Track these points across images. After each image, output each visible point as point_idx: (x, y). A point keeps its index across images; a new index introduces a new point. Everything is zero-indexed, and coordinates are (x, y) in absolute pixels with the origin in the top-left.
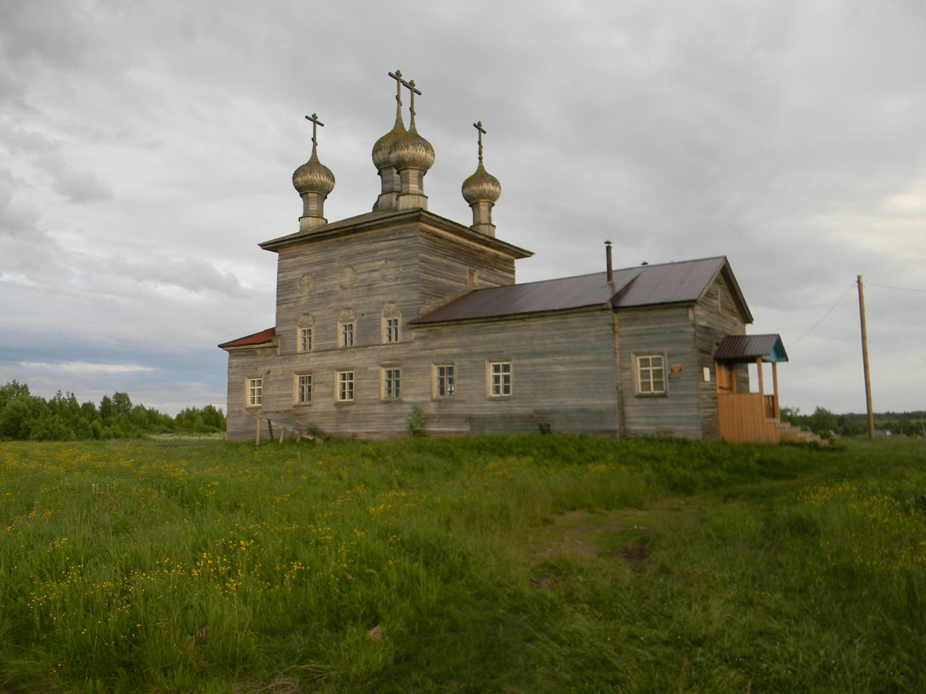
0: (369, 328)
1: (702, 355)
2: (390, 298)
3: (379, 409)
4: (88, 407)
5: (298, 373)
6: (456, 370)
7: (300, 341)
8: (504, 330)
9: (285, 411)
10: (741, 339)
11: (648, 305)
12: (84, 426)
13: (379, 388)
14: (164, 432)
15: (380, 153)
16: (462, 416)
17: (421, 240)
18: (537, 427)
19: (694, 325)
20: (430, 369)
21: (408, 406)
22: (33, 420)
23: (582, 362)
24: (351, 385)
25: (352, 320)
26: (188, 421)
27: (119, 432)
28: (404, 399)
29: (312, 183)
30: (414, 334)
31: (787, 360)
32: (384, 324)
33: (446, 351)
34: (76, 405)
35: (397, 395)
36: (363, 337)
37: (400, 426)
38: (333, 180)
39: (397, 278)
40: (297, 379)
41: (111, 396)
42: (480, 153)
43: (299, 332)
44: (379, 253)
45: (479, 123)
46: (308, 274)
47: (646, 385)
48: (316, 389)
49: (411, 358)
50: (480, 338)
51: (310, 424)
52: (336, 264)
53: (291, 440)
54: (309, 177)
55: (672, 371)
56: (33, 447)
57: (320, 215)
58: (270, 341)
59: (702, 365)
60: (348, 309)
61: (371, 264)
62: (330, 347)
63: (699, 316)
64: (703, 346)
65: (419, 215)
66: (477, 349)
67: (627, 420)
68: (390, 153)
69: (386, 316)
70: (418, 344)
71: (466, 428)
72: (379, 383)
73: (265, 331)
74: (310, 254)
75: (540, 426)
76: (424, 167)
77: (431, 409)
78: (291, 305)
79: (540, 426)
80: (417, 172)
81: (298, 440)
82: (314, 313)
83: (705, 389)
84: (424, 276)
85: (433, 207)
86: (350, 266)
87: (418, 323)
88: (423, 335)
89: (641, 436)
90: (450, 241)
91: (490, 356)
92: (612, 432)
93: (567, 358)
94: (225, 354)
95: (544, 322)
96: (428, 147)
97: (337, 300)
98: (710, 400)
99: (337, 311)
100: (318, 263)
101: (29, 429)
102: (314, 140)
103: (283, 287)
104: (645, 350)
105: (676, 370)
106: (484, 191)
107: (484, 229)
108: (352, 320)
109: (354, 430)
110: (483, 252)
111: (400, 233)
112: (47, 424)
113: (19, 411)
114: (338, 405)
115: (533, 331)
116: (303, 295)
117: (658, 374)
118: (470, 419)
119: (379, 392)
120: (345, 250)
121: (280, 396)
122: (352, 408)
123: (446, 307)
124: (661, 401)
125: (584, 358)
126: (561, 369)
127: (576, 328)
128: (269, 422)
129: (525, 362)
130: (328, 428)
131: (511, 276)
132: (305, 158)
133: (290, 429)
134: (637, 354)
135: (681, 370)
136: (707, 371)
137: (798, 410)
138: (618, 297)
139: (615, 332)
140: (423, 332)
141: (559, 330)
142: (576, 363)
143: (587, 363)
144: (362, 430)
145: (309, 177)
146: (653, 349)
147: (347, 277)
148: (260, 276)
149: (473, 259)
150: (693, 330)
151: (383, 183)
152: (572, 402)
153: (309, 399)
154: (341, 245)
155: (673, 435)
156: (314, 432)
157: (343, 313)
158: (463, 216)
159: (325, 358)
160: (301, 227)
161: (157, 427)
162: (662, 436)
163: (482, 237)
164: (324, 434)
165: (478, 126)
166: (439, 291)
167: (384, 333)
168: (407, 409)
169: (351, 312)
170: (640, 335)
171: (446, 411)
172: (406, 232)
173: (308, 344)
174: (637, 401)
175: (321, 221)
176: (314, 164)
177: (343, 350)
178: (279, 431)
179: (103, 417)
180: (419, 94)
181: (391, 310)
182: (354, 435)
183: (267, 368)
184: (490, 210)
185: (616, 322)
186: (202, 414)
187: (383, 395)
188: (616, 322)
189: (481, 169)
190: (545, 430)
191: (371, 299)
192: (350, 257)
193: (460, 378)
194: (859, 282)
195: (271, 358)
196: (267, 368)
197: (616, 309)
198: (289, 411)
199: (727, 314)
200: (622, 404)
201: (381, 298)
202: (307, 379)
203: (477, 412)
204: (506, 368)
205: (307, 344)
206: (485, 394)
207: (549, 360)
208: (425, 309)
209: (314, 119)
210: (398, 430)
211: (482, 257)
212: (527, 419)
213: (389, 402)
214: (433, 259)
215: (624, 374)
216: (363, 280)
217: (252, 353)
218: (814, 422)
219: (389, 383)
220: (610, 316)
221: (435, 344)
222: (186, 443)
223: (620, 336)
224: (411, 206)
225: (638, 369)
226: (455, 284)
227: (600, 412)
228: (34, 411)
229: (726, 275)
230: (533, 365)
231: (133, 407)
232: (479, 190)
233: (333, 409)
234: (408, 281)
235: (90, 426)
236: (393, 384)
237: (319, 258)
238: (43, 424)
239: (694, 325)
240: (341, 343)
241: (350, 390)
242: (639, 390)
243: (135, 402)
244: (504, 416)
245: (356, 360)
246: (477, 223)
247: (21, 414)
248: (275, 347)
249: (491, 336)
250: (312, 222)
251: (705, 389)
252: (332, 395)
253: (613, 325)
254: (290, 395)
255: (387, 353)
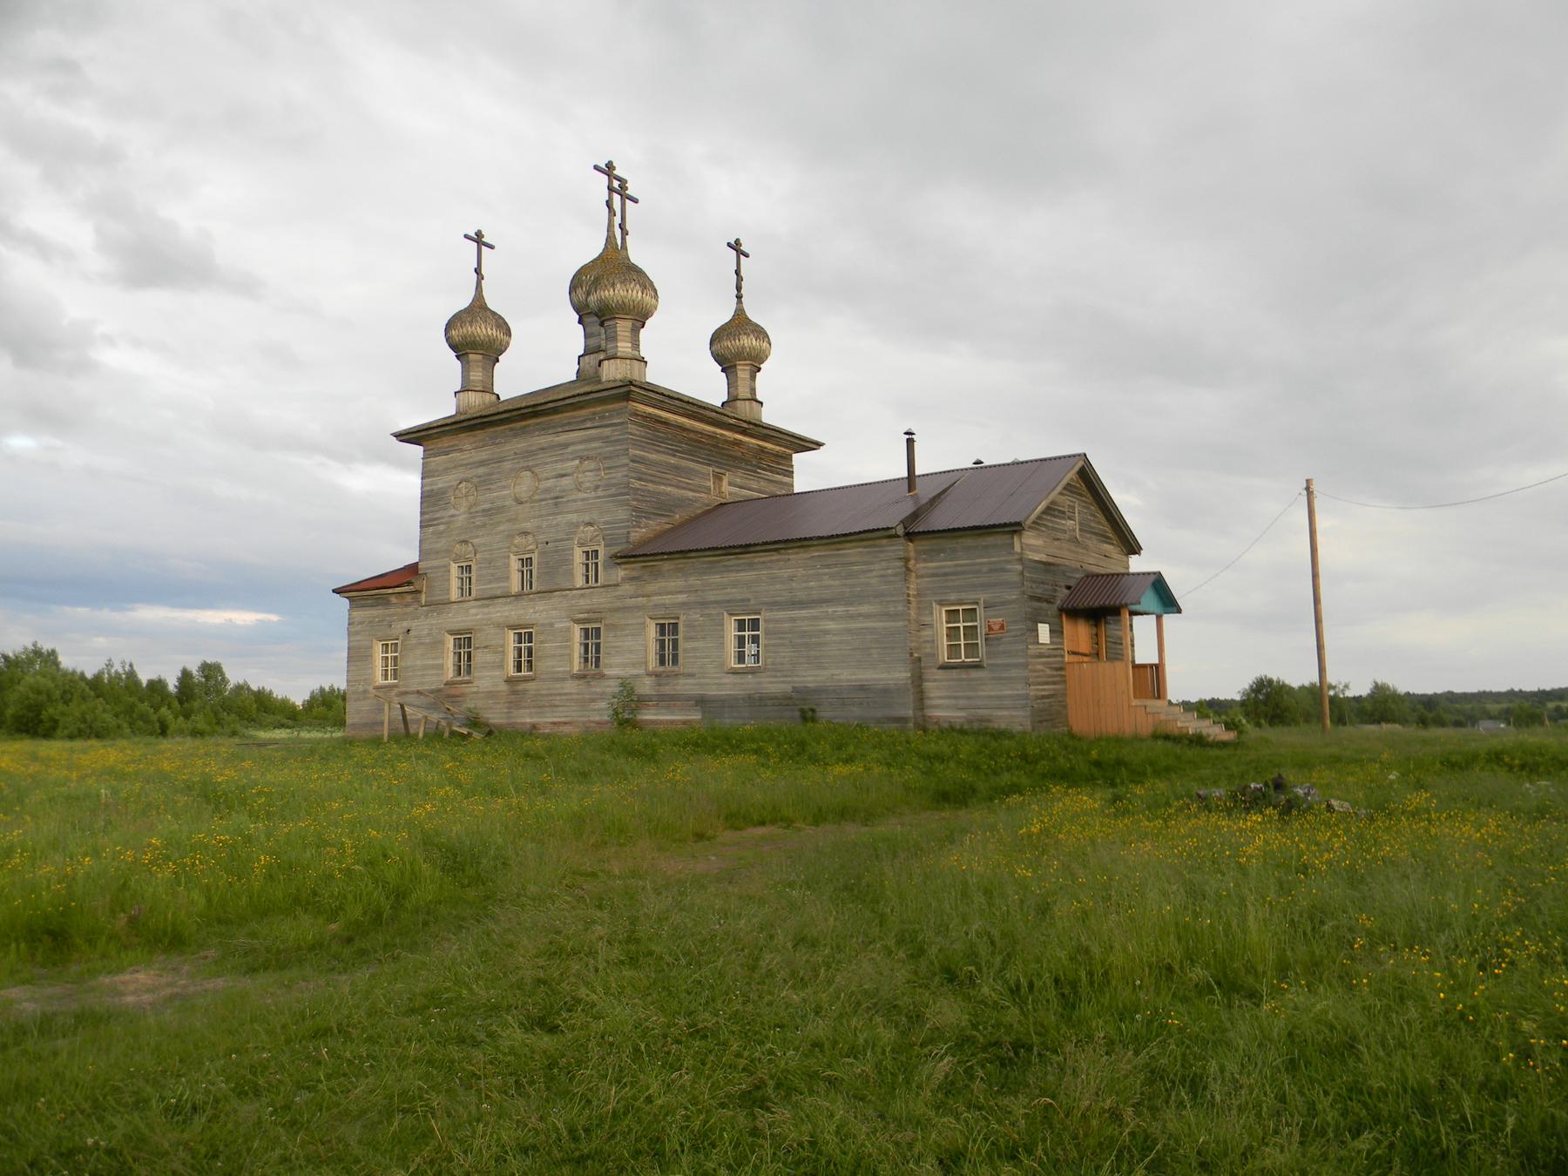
0: (556, 562)
1: (1037, 604)
2: (587, 518)
3: (571, 687)
4: (157, 686)
5: (451, 633)
6: (681, 628)
7: (455, 584)
8: (751, 566)
9: (432, 692)
10: (1119, 578)
11: (954, 530)
12: (144, 717)
13: (570, 655)
14: (282, 726)
15: (579, 291)
16: (688, 698)
17: (632, 428)
18: (797, 714)
19: (1021, 560)
20: (644, 626)
21: (612, 683)
22: (61, 707)
23: (860, 615)
24: (598, 646)
25: (532, 551)
26: (322, 708)
27: (201, 726)
28: (607, 672)
29: (476, 338)
30: (621, 573)
31: (1179, 611)
32: (578, 557)
33: (667, 599)
34: (137, 683)
35: (597, 666)
36: (543, 577)
37: (600, 712)
38: (508, 333)
39: (597, 487)
40: (450, 641)
41: (194, 669)
42: (739, 288)
43: (454, 568)
44: (571, 449)
45: (737, 242)
46: (467, 480)
47: (953, 650)
48: (479, 657)
49: (617, 610)
50: (716, 579)
51: (470, 710)
52: (507, 465)
53: (435, 735)
54: (469, 330)
55: (990, 628)
56: (52, 748)
57: (488, 388)
58: (409, 583)
59: (1036, 619)
60: (526, 533)
61: (559, 466)
62: (498, 593)
63: (1033, 545)
64: (1039, 591)
65: (631, 391)
66: (711, 596)
67: (928, 702)
68: (588, 294)
69: (581, 545)
70: (628, 588)
71: (696, 716)
72: (571, 648)
73: (406, 568)
74: (470, 450)
75: (802, 711)
76: (641, 316)
77: (646, 687)
78: (442, 527)
79: (802, 711)
80: (629, 324)
81: (446, 734)
82: (475, 541)
83: (1041, 656)
84: (637, 484)
85: (656, 375)
86: (528, 469)
87: (623, 558)
88: (634, 574)
89: (946, 725)
90: (683, 428)
91: (731, 606)
92: (902, 720)
93: (840, 609)
94: (343, 603)
95: (807, 555)
96: (646, 284)
97: (509, 521)
98: (1049, 672)
99: (510, 536)
100: (482, 463)
101: (56, 722)
102: (478, 271)
103: (430, 499)
104: (953, 597)
105: (996, 627)
106: (743, 347)
107: (744, 409)
108: (532, 551)
109: (534, 720)
110: (737, 443)
111: (602, 418)
112: (83, 714)
113: (39, 692)
114: (509, 681)
115: (793, 571)
116: (459, 513)
117: (971, 632)
118: (701, 702)
119: (571, 662)
120: (520, 444)
121: (425, 668)
122: (530, 686)
123: (674, 529)
124: (974, 674)
125: (864, 609)
126: (832, 626)
127: (853, 564)
128: (402, 707)
129: (781, 615)
130: (495, 716)
131: (786, 479)
132: (464, 301)
133: (435, 717)
134: (941, 603)
135: (1002, 627)
136: (1044, 631)
137: (1346, 686)
138: (915, 516)
139: (908, 569)
140: (634, 569)
141: (828, 566)
142: (852, 617)
143: (867, 616)
144: (545, 719)
145: (469, 330)
146: (963, 596)
147: (525, 485)
148: (400, 483)
149: (722, 455)
150: (1019, 567)
151: (586, 337)
152: (847, 676)
153: (469, 672)
154: (515, 436)
155: (991, 725)
156: (474, 722)
157: (517, 540)
158: (710, 387)
159: (491, 609)
160: (458, 407)
161: (270, 718)
162: (976, 726)
163: (732, 421)
164: (487, 725)
165: (736, 246)
166: (663, 507)
167: (579, 571)
168: (612, 687)
169: (530, 538)
170: (946, 574)
171: (667, 690)
172: (611, 417)
173: (592, 573)
174: (941, 674)
175: (488, 398)
176: (478, 308)
177: (518, 596)
178: (418, 721)
179: (181, 702)
180: (635, 201)
181: (589, 536)
182: (534, 727)
183: (405, 624)
184: (753, 378)
185: (912, 554)
186: (1243, 703)
187: (577, 666)
188: (912, 554)
189: (740, 314)
190: (808, 716)
191: (560, 518)
192: (529, 454)
193: (687, 639)
194: (1308, 489)
195: (410, 609)
196: (405, 624)
197: (910, 536)
198: (439, 690)
199: (1092, 542)
200: (918, 679)
201: (573, 517)
202: (465, 641)
203: (712, 692)
204: (755, 625)
205: (466, 588)
206: (722, 664)
207: (813, 612)
208: (637, 535)
209: (478, 239)
210: (597, 719)
211: (736, 451)
212: (784, 701)
213: (584, 677)
214: (654, 456)
215: (923, 633)
216: (548, 490)
217: (383, 601)
218: (1369, 707)
219: (662, 643)
220: (900, 547)
221: (651, 588)
222: (275, 742)
223: (918, 577)
224: (619, 377)
225: (943, 626)
226: (690, 494)
227: (886, 691)
228: (65, 692)
229: (1087, 482)
230: (793, 620)
231: (231, 686)
232: (737, 347)
233: (504, 687)
234: (613, 491)
235: (154, 718)
236: (464, 657)
237: (484, 455)
238: (77, 714)
239: (1021, 560)
240: (515, 587)
241: (525, 659)
242: (944, 657)
243: (234, 675)
244: (750, 697)
245: (535, 612)
246: (732, 399)
247: (43, 698)
248: (418, 592)
249: (733, 576)
250: (475, 400)
251: (1041, 656)
252: (501, 666)
253: (907, 560)
254: (441, 667)
255: (582, 602)
